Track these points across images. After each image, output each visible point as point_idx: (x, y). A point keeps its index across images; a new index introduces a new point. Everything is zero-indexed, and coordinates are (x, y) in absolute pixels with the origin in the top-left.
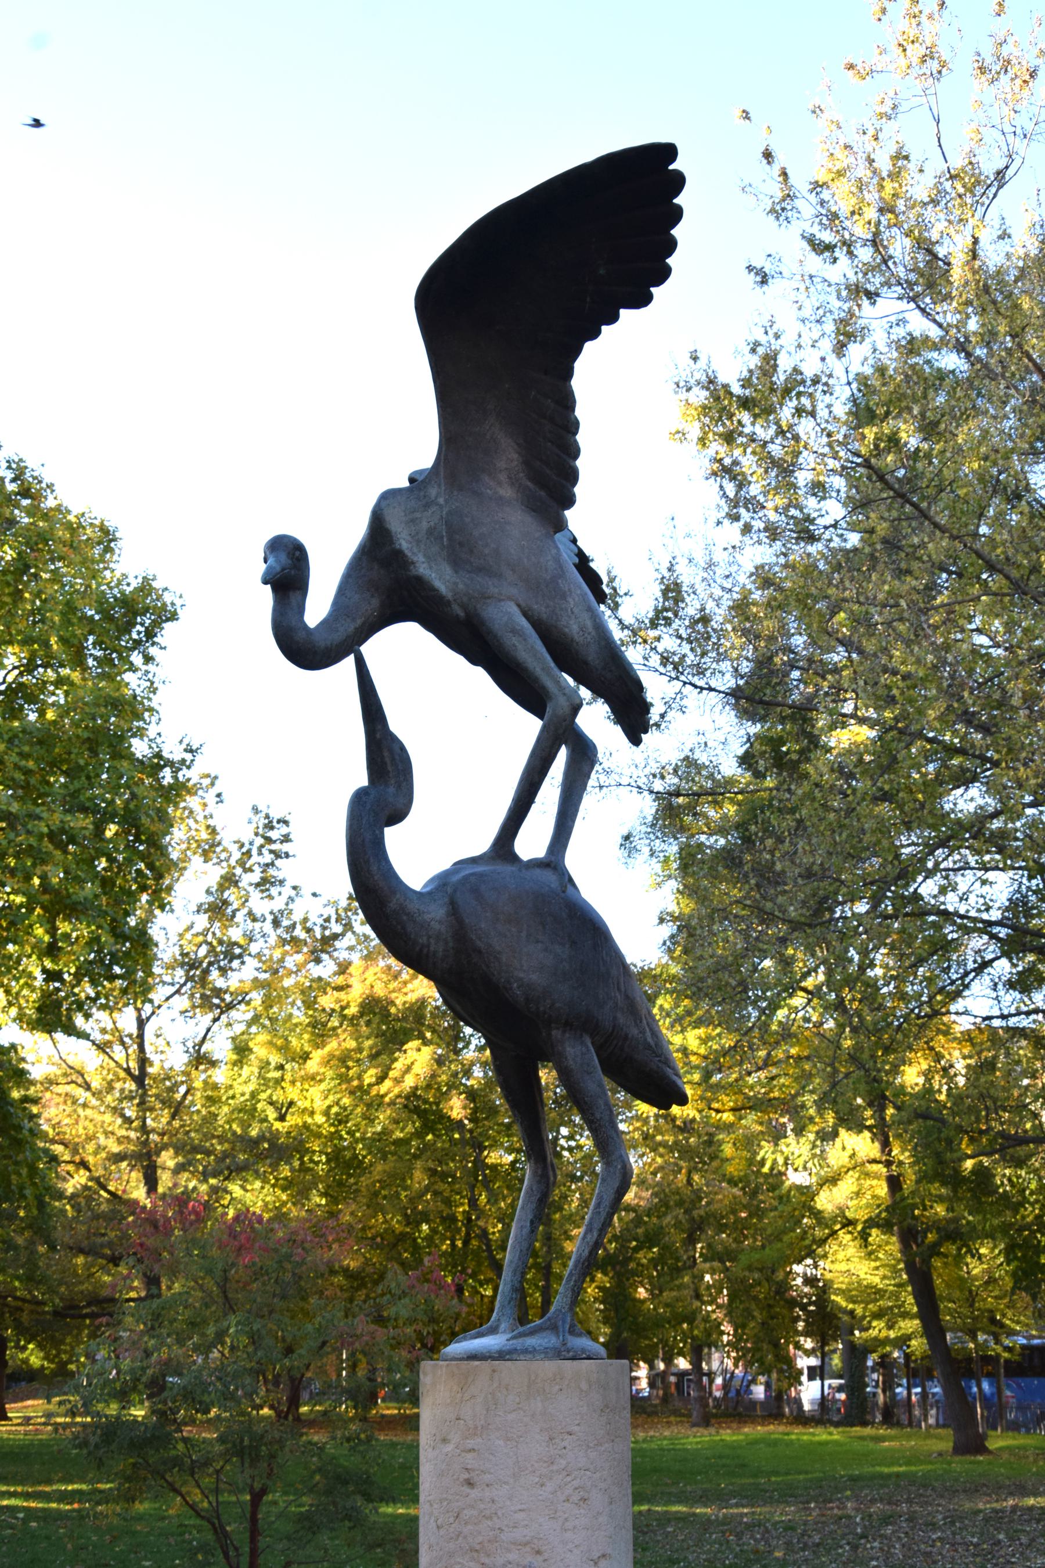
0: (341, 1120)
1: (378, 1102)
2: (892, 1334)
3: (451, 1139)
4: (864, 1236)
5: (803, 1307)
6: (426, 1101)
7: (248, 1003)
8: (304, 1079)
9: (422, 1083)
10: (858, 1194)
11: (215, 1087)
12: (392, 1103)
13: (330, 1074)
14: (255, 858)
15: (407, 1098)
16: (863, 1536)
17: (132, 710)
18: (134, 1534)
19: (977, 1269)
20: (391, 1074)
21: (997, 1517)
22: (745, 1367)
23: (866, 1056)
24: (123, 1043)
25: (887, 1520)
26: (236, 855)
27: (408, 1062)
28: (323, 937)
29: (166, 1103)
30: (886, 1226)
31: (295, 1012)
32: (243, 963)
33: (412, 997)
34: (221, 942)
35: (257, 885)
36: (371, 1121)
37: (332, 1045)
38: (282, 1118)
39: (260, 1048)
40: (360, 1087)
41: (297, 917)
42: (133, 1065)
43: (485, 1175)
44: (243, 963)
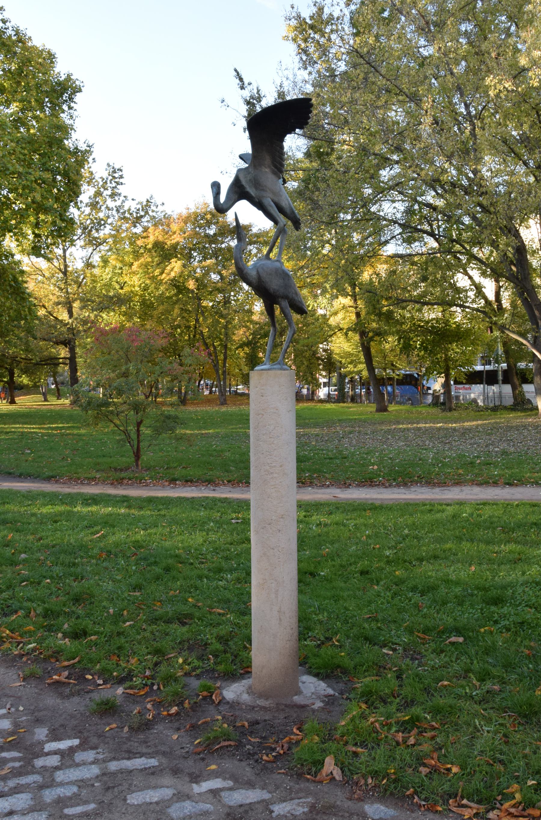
0: (145, 289)
1: (161, 282)
2: (356, 370)
3: (188, 297)
4: (346, 334)
5: (323, 360)
6: (179, 282)
7: (107, 243)
8: (130, 273)
9: (178, 275)
10: (344, 319)
11: (95, 276)
12: (166, 283)
13: (141, 271)
14: (109, 185)
15: (172, 280)
16: (343, 438)
17: (65, 130)
18: (83, 440)
19: (387, 346)
20: (166, 271)
21: (389, 431)
22: (300, 382)
23: (349, 269)
24: (57, 259)
25: (350, 433)
26: (101, 183)
27: (172, 266)
28: (137, 216)
29: (76, 282)
30: (354, 330)
31: (126, 247)
32: (105, 227)
33: (174, 242)
34: (96, 219)
35: (110, 196)
36: (157, 289)
37: (142, 260)
38: (122, 288)
39: (113, 261)
40: (153, 276)
41: (126, 208)
42: (62, 267)
43: (202, 311)
44: (105, 227)
